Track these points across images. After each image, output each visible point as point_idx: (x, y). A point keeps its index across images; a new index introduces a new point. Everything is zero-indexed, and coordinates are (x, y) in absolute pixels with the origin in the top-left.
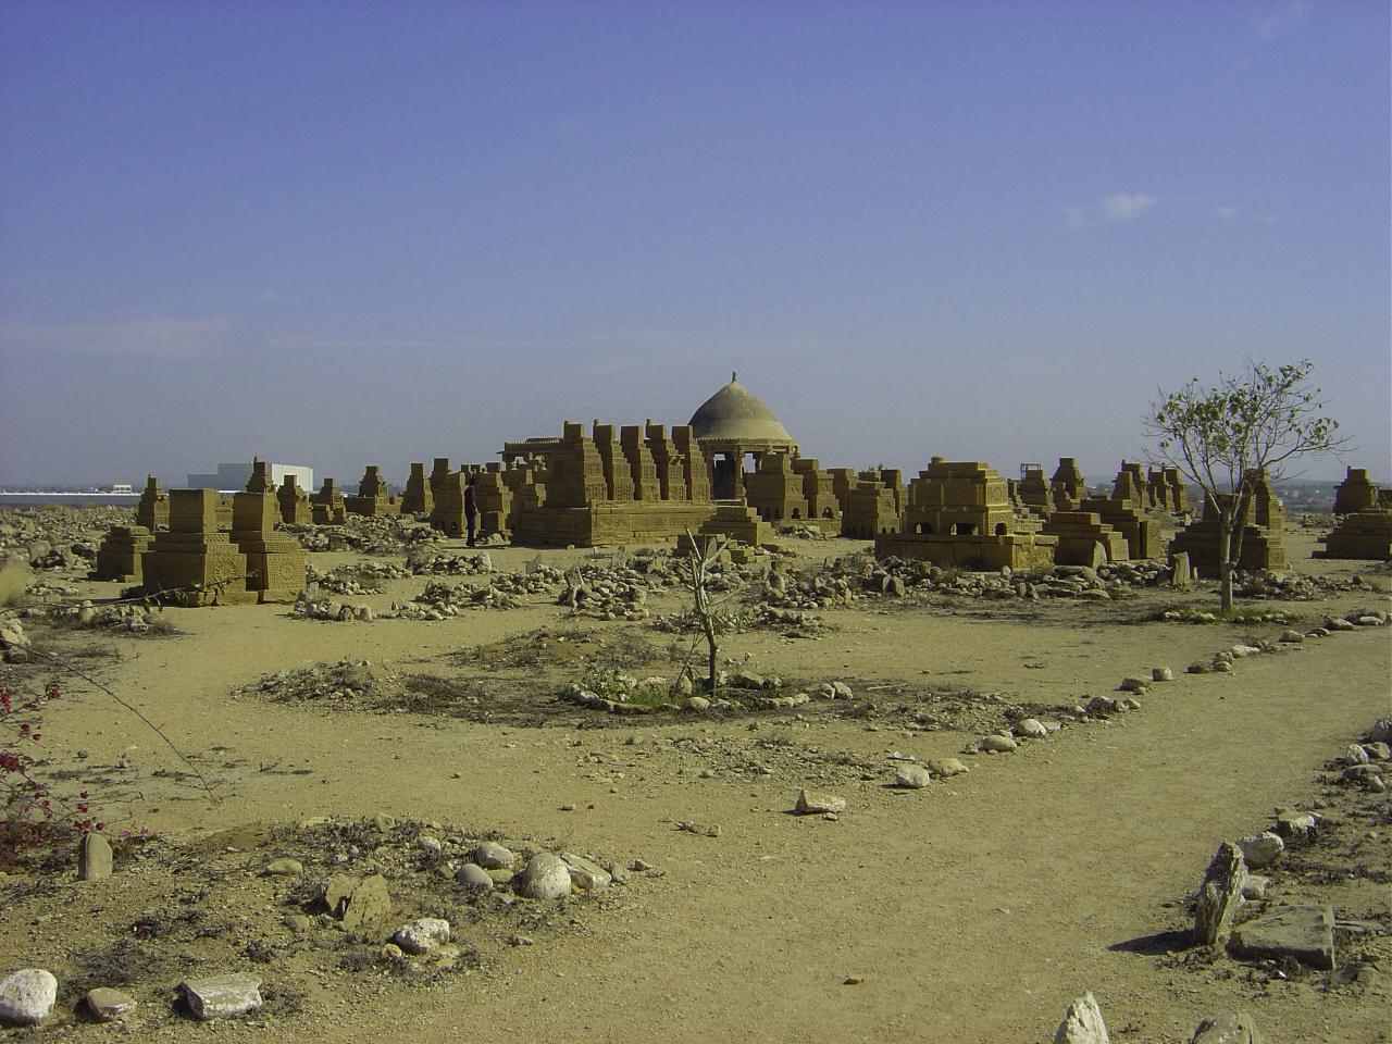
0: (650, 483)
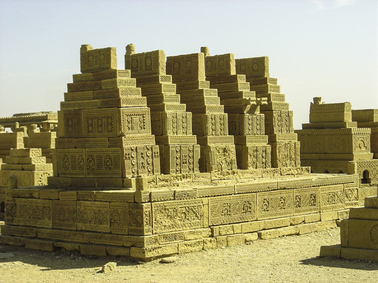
0: (221, 142)
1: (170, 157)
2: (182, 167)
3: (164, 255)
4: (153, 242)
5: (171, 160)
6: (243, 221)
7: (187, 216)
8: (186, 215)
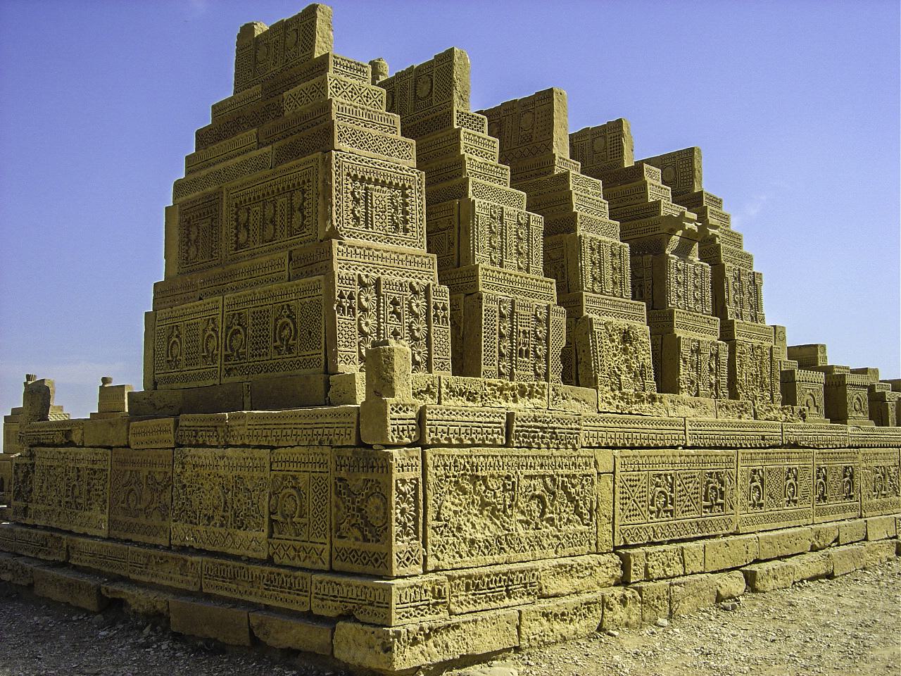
0: (614, 314)
1: (481, 327)
2: (516, 365)
3: (467, 655)
4: (428, 605)
5: (483, 339)
6: (704, 534)
7: (547, 510)
8: (545, 506)
